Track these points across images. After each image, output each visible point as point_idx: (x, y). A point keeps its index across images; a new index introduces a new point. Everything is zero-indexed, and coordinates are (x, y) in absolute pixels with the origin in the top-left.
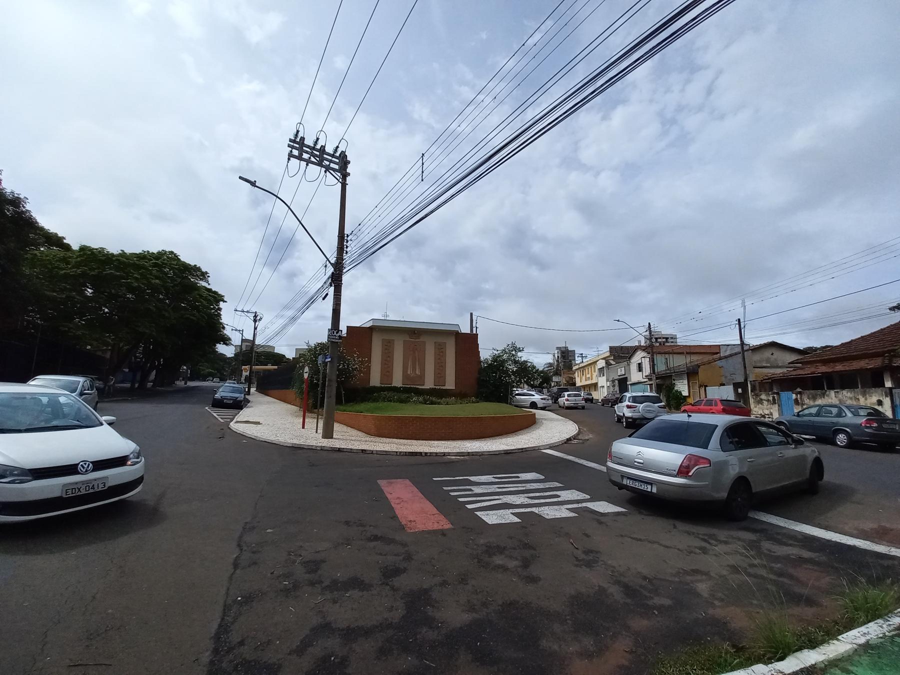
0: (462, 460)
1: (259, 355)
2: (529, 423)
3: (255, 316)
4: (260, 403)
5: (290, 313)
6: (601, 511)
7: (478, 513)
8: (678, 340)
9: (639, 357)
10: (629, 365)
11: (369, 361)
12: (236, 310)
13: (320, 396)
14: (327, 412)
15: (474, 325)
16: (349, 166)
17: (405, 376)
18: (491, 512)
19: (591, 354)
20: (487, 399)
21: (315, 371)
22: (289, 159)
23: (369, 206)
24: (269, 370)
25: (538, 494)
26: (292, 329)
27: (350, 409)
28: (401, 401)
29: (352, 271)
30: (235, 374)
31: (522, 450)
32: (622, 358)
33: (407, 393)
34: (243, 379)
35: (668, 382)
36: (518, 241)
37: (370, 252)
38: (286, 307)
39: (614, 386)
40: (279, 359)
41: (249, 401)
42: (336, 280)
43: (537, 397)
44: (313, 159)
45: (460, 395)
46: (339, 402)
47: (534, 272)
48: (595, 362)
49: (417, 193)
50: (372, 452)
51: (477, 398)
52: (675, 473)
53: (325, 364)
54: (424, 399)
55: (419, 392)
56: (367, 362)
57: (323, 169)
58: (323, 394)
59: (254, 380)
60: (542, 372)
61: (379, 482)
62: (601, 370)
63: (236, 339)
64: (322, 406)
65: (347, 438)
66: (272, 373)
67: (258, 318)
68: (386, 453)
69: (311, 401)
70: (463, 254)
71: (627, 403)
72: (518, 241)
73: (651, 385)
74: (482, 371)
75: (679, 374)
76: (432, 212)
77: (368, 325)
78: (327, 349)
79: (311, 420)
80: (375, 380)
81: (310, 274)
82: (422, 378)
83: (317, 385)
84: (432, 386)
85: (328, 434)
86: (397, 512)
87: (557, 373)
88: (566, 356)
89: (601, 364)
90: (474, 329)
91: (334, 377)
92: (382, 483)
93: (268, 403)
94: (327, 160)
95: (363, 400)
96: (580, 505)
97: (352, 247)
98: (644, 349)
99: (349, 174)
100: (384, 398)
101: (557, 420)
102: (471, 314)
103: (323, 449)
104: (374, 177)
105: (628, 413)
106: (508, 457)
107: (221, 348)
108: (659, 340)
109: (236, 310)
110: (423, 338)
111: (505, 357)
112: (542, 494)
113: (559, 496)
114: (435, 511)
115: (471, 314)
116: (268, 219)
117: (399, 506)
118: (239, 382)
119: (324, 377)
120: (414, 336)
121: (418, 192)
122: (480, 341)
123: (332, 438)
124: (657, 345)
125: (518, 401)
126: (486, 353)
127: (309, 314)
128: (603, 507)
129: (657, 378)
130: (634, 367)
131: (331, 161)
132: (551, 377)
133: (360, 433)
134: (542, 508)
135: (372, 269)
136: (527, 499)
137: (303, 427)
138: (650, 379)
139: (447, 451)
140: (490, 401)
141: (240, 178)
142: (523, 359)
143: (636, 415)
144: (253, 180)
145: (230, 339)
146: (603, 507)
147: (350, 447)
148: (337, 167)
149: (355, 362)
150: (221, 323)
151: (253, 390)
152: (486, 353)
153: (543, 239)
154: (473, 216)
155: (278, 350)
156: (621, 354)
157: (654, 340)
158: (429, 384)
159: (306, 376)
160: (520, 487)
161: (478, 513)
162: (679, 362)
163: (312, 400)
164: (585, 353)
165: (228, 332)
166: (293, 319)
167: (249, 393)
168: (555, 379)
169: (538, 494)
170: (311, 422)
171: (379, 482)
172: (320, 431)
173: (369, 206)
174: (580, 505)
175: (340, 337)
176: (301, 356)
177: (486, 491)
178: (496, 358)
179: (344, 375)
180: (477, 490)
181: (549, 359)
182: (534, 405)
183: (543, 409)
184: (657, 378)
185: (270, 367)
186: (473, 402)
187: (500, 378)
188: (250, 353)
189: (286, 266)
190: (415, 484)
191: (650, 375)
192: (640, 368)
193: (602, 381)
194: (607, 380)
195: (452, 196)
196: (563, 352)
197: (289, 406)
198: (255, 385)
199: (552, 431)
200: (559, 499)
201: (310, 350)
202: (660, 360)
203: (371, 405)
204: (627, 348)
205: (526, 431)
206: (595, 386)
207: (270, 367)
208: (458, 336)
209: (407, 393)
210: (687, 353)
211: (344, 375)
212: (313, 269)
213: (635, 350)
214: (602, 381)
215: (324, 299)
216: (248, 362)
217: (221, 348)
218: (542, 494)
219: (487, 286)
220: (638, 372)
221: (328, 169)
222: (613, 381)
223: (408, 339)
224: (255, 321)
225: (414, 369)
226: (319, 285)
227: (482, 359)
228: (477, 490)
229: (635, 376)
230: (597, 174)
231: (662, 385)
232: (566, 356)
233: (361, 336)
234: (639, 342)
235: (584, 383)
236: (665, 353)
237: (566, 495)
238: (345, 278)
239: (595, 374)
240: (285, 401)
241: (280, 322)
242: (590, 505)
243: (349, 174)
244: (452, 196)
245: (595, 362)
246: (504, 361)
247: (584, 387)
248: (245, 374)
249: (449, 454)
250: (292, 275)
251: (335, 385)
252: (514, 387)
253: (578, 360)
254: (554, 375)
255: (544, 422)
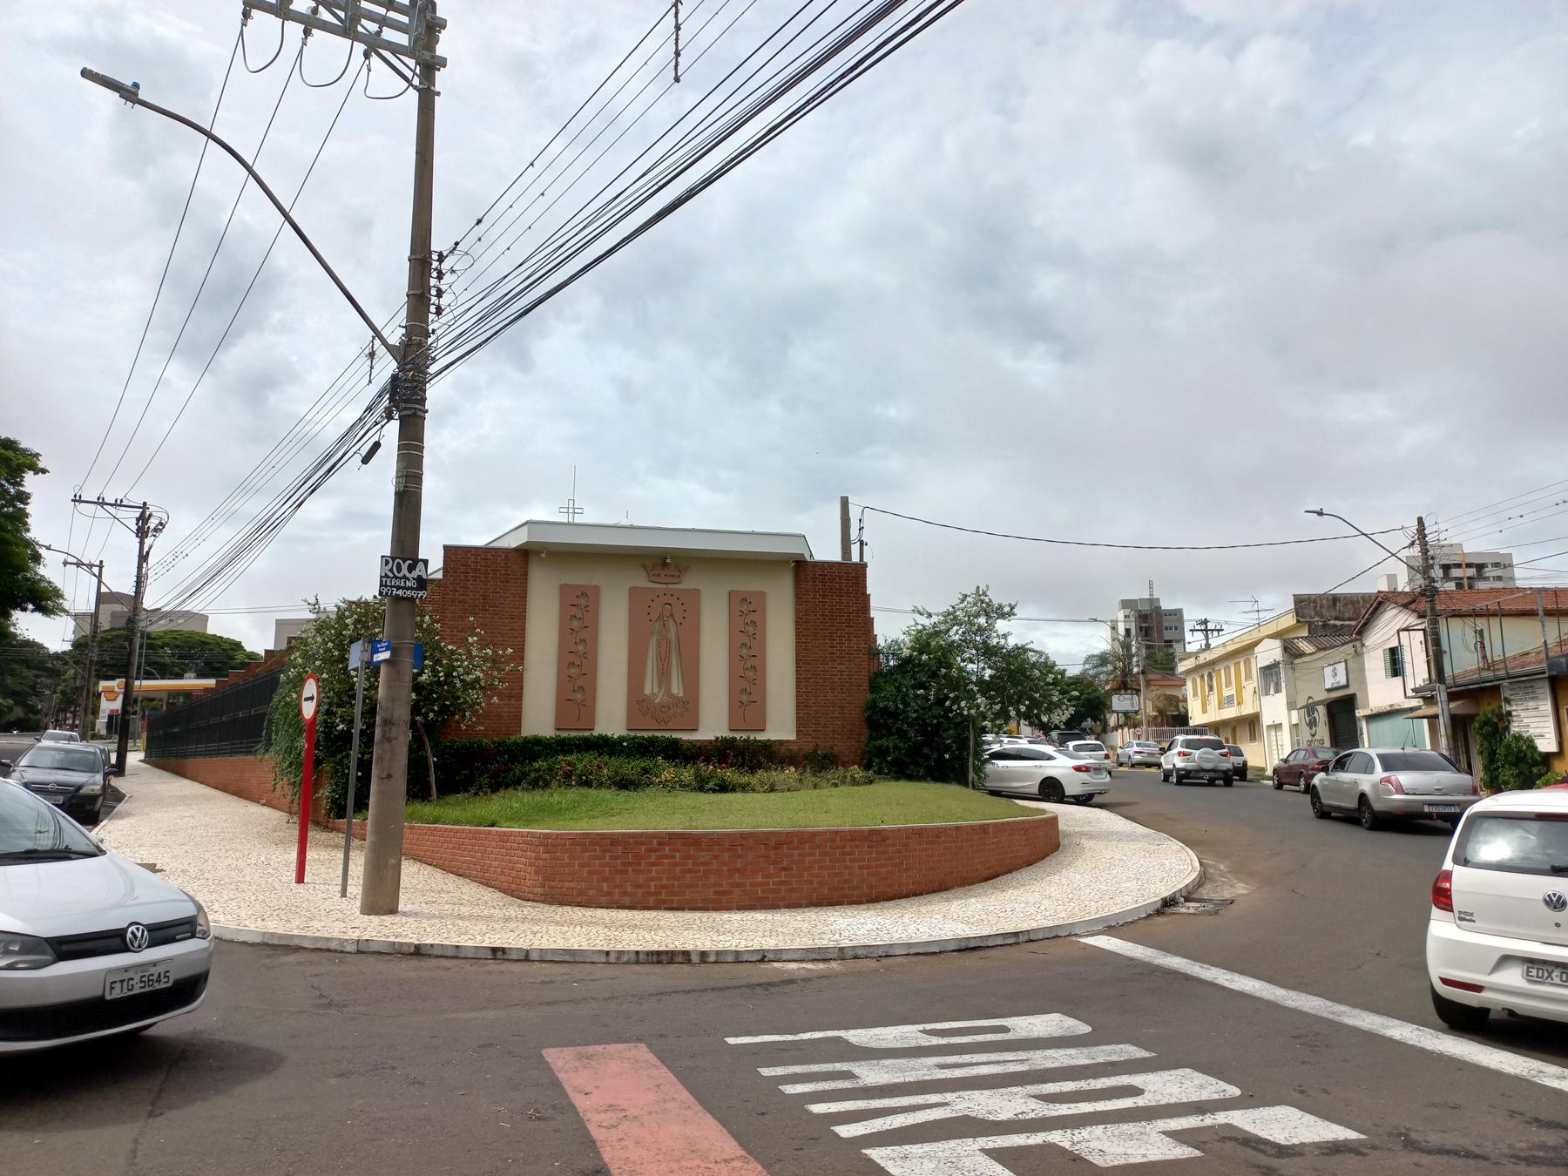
0: (822, 977)
1: (152, 643)
2: (1038, 847)
3: (143, 519)
4: (159, 802)
5: (256, 507)
6: (1279, 1135)
7: (875, 1154)
8: (1518, 573)
9: (1389, 628)
10: (1358, 654)
11: (519, 656)
12: (77, 500)
13: (354, 773)
14: (381, 828)
15: (854, 534)
16: (443, 36)
17: (637, 704)
18: (915, 1149)
19: (1234, 621)
20: (902, 770)
21: (339, 694)
22: (246, 15)
23: (511, 163)
24: (188, 694)
25: (1068, 1086)
26: (262, 561)
27: (456, 813)
28: (624, 784)
29: (460, 370)
30: (74, 708)
31: (1017, 939)
32: (1338, 631)
33: (649, 756)
34: (101, 722)
35: (1486, 709)
36: (986, 267)
37: (519, 306)
38: (245, 487)
39: (1312, 724)
40: (218, 656)
41: (119, 797)
42: (405, 399)
43: (1061, 764)
44: (324, 15)
45: (813, 760)
46: (418, 790)
47: (1038, 370)
48: (1249, 649)
49: (661, 116)
50: (526, 957)
51: (867, 767)
52: (1035, 790)
53: (373, 669)
54: (697, 776)
55: (677, 753)
56: (511, 658)
57: (360, 48)
58: (365, 766)
59: (137, 724)
60: (1077, 682)
61: (550, 1054)
62: (1269, 671)
63: (79, 595)
64: (361, 804)
65: (446, 909)
66: (196, 705)
67: (152, 523)
68: (571, 958)
69: (325, 792)
70: (808, 312)
71: (1179, 749)
72: (986, 267)
73: (1433, 719)
74: (877, 680)
75: (1525, 682)
76: (708, 181)
77: (513, 542)
78: (379, 620)
79: (324, 854)
80: (539, 718)
81: (319, 378)
82: (689, 707)
83: (347, 736)
84: (722, 732)
85: (382, 898)
86: (607, 1154)
87: (1125, 684)
88: (1153, 630)
89: (1270, 652)
90: (855, 549)
91: (403, 713)
92: (559, 1059)
93: (184, 800)
94: (372, 17)
95: (498, 784)
96: (1208, 1120)
97: (458, 294)
98: (1408, 602)
99: (443, 63)
100: (568, 775)
101: (1131, 837)
102: (845, 503)
103: (363, 950)
104: (522, 68)
105: (1180, 763)
106: (969, 961)
107: (28, 625)
108: (1455, 573)
109: (77, 500)
110: (689, 583)
111: (955, 635)
112: (1082, 1085)
113: (1135, 1091)
114: (731, 1147)
115: (845, 503)
116: (182, 208)
117: (614, 1135)
118: (88, 733)
119: (370, 711)
120: (665, 571)
121: (664, 113)
122: (875, 586)
123: (393, 910)
124: (1448, 590)
125: (1001, 776)
126: (892, 626)
127: (318, 508)
128: (1285, 1125)
129: (1452, 697)
130: (1375, 663)
131: (383, 22)
132: (1109, 694)
133: (489, 895)
134: (1085, 1133)
135: (523, 361)
136: (1033, 1104)
137: (300, 878)
138: (1430, 700)
139: (770, 944)
140: (910, 778)
141: (86, 73)
142: (1011, 642)
143: (1191, 765)
144: (128, 83)
145: (57, 594)
146: (1285, 1125)
147: (455, 940)
148: (403, 39)
149: (471, 660)
150: (29, 544)
151: (134, 758)
152: (892, 626)
153: (1067, 257)
154: (845, 189)
155: (217, 627)
156: (1333, 620)
157: (1437, 573)
158: (713, 725)
159: (308, 710)
160: (1014, 1063)
161: (875, 1154)
162: (1521, 641)
163: (328, 788)
164: (1214, 617)
165: (50, 570)
166: (267, 527)
167: (120, 769)
168: (1120, 703)
169: (1068, 1086)
170: (325, 858)
171: (550, 1054)
172: (356, 889)
173: (511, 163)
174: (1208, 1120)
175: (422, 583)
176: (294, 644)
177: (910, 1077)
178: (923, 641)
179: (436, 708)
180: (871, 1074)
181: (1098, 640)
182: (1051, 789)
183: (1084, 800)
184: (1452, 697)
185: (190, 682)
186: (854, 782)
187: (940, 702)
188: (125, 641)
189: (240, 356)
190: (667, 1058)
191: (1429, 686)
192: (1395, 665)
193: (1275, 709)
194: (1291, 705)
195: (773, 131)
196: (1143, 617)
197: (254, 809)
198: (141, 743)
199: (1113, 872)
200: (1140, 1101)
201: (321, 626)
202: (1459, 637)
203: (521, 799)
204: (1352, 601)
205: (1025, 874)
206: (1251, 723)
207: (190, 682)
208: (802, 569)
209: (649, 756)
210: (1549, 613)
211: (436, 708)
212: (333, 370)
213: (1375, 605)
214: (1275, 709)
215: (366, 460)
216: (120, 668)
217: (28, 625)
218: (1082, 1085)
219: (895, 412)
220: (1389, 677)
221: (374, 46)
222: (1310, 709)
223: (641, 581)
224: (142, 533)
225: (664, 676)
226: (352, 414)
227: (881, 642)
228: (871, 1074)
229: (1381, 692)
230: (1236, 47)
231: (1470, 718)
232: (1153, 630)
233: (494, 576)
234: (1392, 578)
235: (1215, 715)
236: (1476, 614)
237: (1163, 1086)
238: (436, 393)
239: (1250, 687)
240: (241, 793)
241: (225, 536)
242: (1242, 1119)
243: (443, 63)
244: (773, 131)
245: (1249, 649)
246: (952, 648)
247: (1216, 727)
248: (110, 705)
249: (779, 955)
250: (259, 386)
251: (404, 737)
252: (984, 731)
253: (1194, 642)
254: (1116, 690)
255: (1087, 843)
